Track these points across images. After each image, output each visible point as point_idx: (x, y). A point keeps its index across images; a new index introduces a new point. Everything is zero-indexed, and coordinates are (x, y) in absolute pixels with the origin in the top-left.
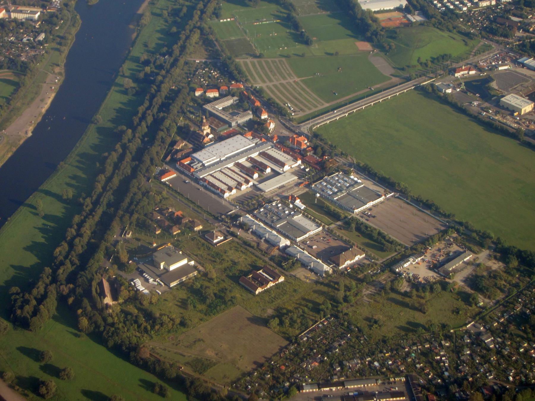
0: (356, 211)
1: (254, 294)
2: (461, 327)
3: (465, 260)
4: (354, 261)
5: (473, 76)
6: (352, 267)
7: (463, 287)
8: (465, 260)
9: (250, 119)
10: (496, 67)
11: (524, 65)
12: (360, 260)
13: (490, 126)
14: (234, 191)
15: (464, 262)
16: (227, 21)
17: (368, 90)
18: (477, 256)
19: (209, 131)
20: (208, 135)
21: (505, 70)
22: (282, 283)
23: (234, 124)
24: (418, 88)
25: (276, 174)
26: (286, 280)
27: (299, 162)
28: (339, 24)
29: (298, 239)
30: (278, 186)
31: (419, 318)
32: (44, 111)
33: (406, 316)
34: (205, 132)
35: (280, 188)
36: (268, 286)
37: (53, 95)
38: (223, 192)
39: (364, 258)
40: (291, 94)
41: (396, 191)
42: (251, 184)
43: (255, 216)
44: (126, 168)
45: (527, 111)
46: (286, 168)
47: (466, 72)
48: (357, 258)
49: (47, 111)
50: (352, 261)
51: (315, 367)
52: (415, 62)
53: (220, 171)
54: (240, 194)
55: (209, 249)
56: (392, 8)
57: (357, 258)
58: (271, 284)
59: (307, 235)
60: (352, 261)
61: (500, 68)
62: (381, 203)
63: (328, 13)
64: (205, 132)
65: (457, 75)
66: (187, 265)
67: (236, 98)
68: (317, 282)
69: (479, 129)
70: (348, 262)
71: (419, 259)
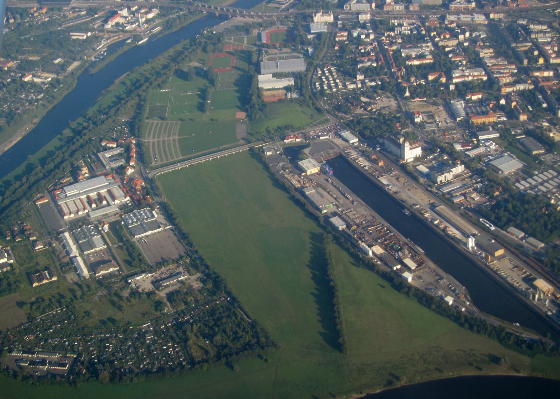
0: (137, 237)
1: (32, 284)
2: (140, 325)
3: (179, 279)
4: (109, 271)
5: (299, 142)
6: (104, 276)
7: (163, 298)
8: (179, 279)
9: (122, 165)
10: (319, 136)
11: (341, 137)
12: (113, 271)
13: (283, 186)
14: (72, 215)
15: (178, 281)
16: (165, 92)
17: (217, 148)
18: (190, 277)
19: (87, 171)
20: (85, 173)
21: (325, 139)
22: (55, 281)
23: (107, 167)
24: (251, 149)
25: (109, 205)
26: (58, 280)
27: (128, 198)
28: (315, 301)
29: (86, 253)
30: (104, 213)
31: (118, 316)
32: (6, 149)
33: (111, 312)
34: (83, 172)
35: (103, 215)
36: (44, 282)
37: (20, 138)
38: (65, 215)
39: (118, 270)
40: (164, 148)
41: (173, 224)
42: (86, 211)
43: (457, 12)
44: (19, 193)
45: (313, 173)
46: (117, 202)
47: (294, 139)
48: (111, 270)
49: (9, 150)
50: (107, 272)
51: (30, 340)
52: (263, 130)
53: (74, 201)
54: (77, 217)
55: (29, 252)
56: (281, 87)
57: (111, 270)
58: (45, 281)
59: (93, 250)
60: (107, 272)
61: (321, 138)
62: (159, 232)
63: (237, 88)
64: (83, 172)
65: (286, 141)
66: (6, 263)
67: (122, 149)
68: (76, 283)
69: (269, 183)
70: (103, 272)
71: (150, 275)
